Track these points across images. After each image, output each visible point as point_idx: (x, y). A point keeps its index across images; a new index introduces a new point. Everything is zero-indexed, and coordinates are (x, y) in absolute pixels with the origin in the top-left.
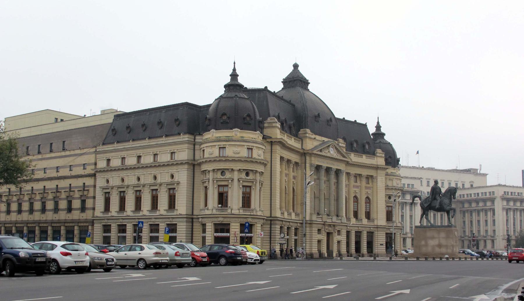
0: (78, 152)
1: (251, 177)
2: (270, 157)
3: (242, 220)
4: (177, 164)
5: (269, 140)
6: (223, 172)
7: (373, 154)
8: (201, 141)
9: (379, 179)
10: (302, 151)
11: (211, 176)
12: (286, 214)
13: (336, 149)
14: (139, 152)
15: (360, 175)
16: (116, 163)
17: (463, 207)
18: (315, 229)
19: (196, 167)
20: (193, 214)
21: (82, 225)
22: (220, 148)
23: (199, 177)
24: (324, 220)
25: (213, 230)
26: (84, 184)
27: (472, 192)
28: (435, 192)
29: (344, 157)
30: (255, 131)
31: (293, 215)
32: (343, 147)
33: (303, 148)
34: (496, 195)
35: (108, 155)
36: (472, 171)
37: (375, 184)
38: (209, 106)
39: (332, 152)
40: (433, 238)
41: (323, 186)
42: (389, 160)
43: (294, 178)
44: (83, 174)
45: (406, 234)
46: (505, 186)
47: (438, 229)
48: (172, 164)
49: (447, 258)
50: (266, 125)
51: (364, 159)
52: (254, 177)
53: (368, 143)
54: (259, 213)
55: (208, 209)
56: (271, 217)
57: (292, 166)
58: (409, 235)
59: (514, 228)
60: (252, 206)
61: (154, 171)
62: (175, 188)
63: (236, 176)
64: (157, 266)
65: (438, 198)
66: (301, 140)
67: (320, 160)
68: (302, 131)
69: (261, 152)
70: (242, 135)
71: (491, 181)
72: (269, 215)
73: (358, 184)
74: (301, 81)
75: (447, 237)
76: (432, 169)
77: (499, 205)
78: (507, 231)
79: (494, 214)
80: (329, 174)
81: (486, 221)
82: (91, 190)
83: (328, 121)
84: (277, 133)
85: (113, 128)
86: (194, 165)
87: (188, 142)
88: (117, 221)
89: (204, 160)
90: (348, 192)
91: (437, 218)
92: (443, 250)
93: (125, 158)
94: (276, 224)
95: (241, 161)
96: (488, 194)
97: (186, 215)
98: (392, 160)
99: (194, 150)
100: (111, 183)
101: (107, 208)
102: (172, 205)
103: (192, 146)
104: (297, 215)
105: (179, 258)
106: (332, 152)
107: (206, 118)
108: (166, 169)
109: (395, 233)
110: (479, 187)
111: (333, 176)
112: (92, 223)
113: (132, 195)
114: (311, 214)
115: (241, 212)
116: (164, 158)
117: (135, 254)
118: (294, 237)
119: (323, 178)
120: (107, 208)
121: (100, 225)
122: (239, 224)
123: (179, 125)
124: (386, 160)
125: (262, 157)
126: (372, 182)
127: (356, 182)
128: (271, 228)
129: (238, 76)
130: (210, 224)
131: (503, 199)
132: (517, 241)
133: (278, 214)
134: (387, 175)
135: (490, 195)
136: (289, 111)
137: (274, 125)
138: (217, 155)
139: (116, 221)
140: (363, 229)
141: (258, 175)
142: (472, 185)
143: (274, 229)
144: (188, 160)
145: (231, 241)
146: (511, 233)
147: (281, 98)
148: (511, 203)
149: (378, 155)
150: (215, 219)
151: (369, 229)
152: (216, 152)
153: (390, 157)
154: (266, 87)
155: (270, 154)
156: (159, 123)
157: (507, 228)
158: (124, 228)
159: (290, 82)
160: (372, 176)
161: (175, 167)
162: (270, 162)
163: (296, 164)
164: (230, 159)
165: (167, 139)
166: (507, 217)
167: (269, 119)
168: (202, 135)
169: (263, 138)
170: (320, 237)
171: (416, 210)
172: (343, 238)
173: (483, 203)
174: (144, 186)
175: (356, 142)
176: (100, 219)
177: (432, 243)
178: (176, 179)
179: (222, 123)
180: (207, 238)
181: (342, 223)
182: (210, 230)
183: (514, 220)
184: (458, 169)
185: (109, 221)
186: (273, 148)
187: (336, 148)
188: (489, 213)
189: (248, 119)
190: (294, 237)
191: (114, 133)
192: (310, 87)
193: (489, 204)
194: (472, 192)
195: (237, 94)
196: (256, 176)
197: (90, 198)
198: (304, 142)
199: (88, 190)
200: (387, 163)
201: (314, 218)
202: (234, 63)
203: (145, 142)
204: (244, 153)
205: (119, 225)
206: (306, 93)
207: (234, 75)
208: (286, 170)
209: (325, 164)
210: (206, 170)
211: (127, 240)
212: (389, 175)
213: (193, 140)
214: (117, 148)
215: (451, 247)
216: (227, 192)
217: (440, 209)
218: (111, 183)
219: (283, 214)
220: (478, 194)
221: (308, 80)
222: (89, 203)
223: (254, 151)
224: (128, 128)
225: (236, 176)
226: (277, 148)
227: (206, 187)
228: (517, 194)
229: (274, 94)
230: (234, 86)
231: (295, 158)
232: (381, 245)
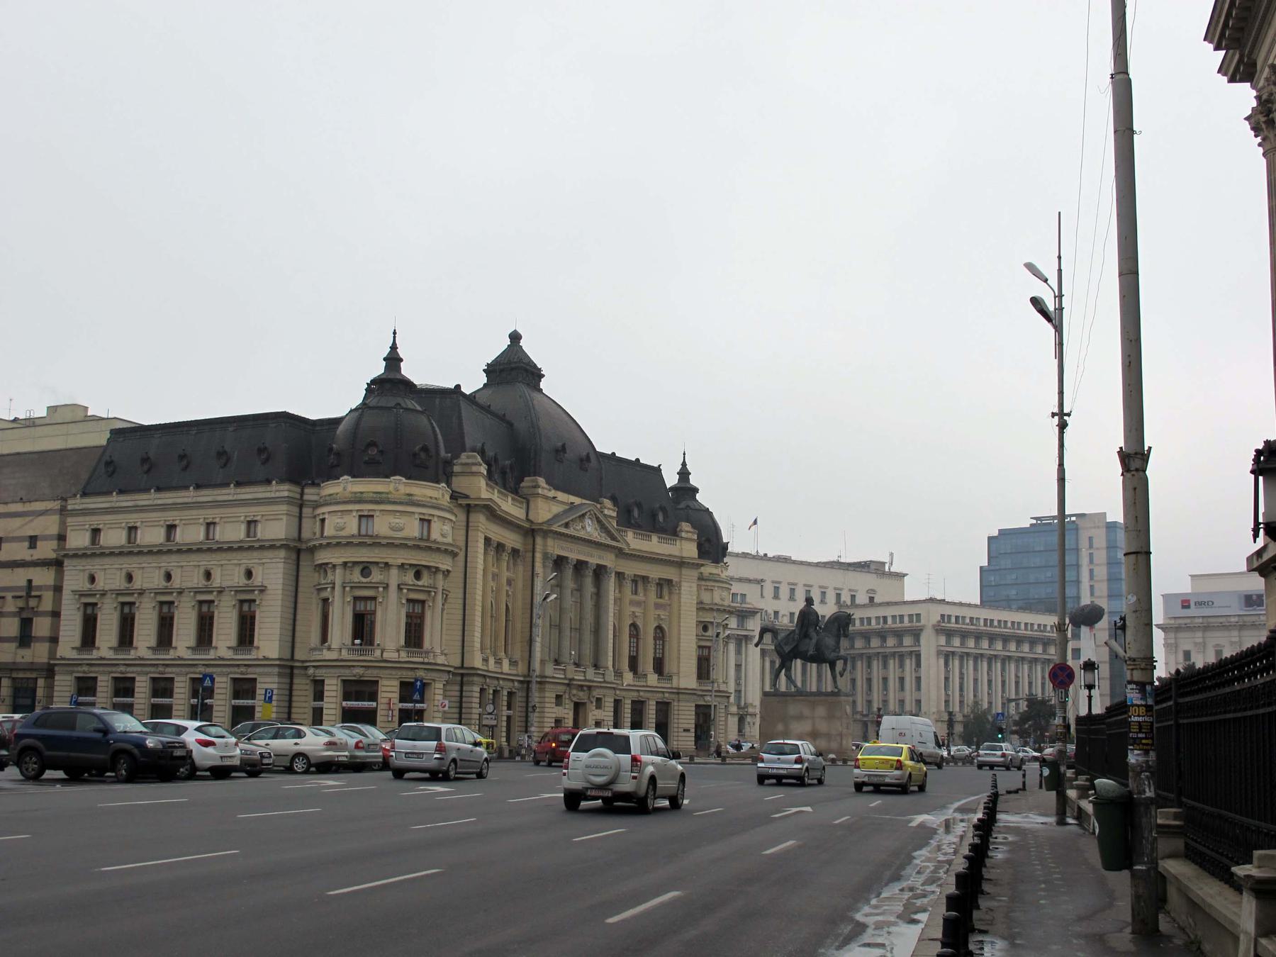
0: (18, 507)
1: (425, 581)
3: (405, 673)
4: (262, 548)
5: (464, 502)
6: (366, 569)
7: (672, 532)
8: (315, 498)
9: (685, 587)
10: (527, 525)
11: (338, 576)
12: (492, 661)
13: (599, 521)
14: (171, 517)
15: (645, 579)
16: (114, 537)
18: (550, 696)
19: (302, 556)
20: (292, 659)
21: (21, 675)
22: (360, 516)
23: (309, 578)
24: (570, 676)
25: (340, 694)
26: (30, 581)
27: (873, 613)
29: (614, 539)
30: (438, 482)
31: (506, 664)
33: (531, 517)
34: (923, 622)
35: (95, 521)
36: (873, 567)
37: (675, 597)
38: (336, 422)
39: (590, 529)
40: (800, 717)
41: (569, 601)
42: (707, 545)
43: (509, 582)
44: (28, 558)
46: (943, 601)
47: (812, 698)
48: (251, 548)
49: (833, 761)
50: (456, 469)
51: (654, 545)
52: (431, 582)
53: (663, 509)
54: (441, 660)
55: (329, 649)
57: (505, 557)
59: (961, 695)
60: (427, 645)
61: (205, 561)
62: (254, 601)
63: (394, 577)
64: (326, 767)
65: (813, 634)
66: (525, 499)
67: (565, 545)
68: (527, 482)
69: (447, 528)
70: (408, 490)
71: (913, 590)
72: (458, 664)
73: (641, 597)
74: (526, 371)
75: (830, 717)
76: (785, 560)
77: (929, 645)
78: (947, 702)
79: (918, 665)
80: (582, 576)
81: (902, 680)
82: (48, 596)
84: (481, 488)
85: (106, 458)
86: (299, 552)
87: (289, 501)
88: (114, 669)
89: (324, 542)
90: (619, 615)
91: (805, 675)
93: (136, 528)
94: (472, 683)
95: (405, 546)
96: (906, 619)
97: (279, 659)
98: (712, 545)
99: (300, 518)
100: (100, 584)
101: (88, 639)
102: (246, 635)
103: (296, 510)
104: (513, 663)
105: (362, 753)
106: (590, 529)
107: (331, 449)
108: (236, 557)
110: (888, 604)
111: (589, 582)
112: (49, 671)
113: (151, 611)
114: (543, 662)
116: (232, 532)
117: (286, 745)
118: (505, 712)
119: (570, 583)
120: (88, 639)
121: (68, 678)
122: (397, 683)
123: (267, 460)
124: (700, 547)
125: (449, 540)
126: (670, 593)
127: (636, 593)
128: (461, 691)
130: (334, 681)
131: (939, 630)
132: (966, 726)
133: (478, 663)
134: (701, 578)
135: (911, 621)
136: (491, 435)
137: (474, 469)
138: (355, 532)
139: (109, 669)
140: (648, 695)
141: (440, 576)
142: (871, 599)
144: (286, 539)
145: (379, 718)
146: (956, 708)
147: (486, 409)
148: (956, 642)
149: (683, 535)
150: (347, 671)
152: (351, 526)
153: (708, 540)
155: (464, 532)
156: (221, 454)
157: (947, 695)
158: (128, 684)
159: (502, 371)
160: (669, 582)
161: (255, 554)
163: (515, 552)
164: (384, 542)
165: (238, 490)
166: (947, 672)
167: (464, 455)
168: (318, 485)
169: (451, 497)
173: (899, 638)
174: (180, 593)
175: (639, 505)
176: (70, 665)
178: (258, 579)
179: (366, 463)
180: (325, 711)
182: (334, 694)
183: (962, 678)
184: (842, 560)
185: (93, 669)
187: (597, 518)
188: (908, 662)
189: (423, 455)
190: (505, 712)
191: (111, 469)
192: (543, 384)
193: (908, 641)
194: (873, 613)
195: (399, 400)
197: (44, 614)
198: (532, 505)
199: (39, 597)
200: (703, 553)
201: (550, 670)
202: (395, 333)
203: (187, 494)
204: (412, 529)
205: (115, 679)
206: (535, 395)
207: (393, 360)
208: (508, 569)
209: (574, 553)
211: (215, 714)
213: (298, 496)
214: (117, 504)
216: (374, 613)
217: (818, 658)
218: (100, 584)
219: (486, 660)
222: (41, 627)
223: (433, 524)
224: (145, 460)
225: (394, 577)
226: (480, 520)
227: (325, 601)
228: (968, 621)
229: (471, 399)
230: (390, 384)
231: (511, 539)
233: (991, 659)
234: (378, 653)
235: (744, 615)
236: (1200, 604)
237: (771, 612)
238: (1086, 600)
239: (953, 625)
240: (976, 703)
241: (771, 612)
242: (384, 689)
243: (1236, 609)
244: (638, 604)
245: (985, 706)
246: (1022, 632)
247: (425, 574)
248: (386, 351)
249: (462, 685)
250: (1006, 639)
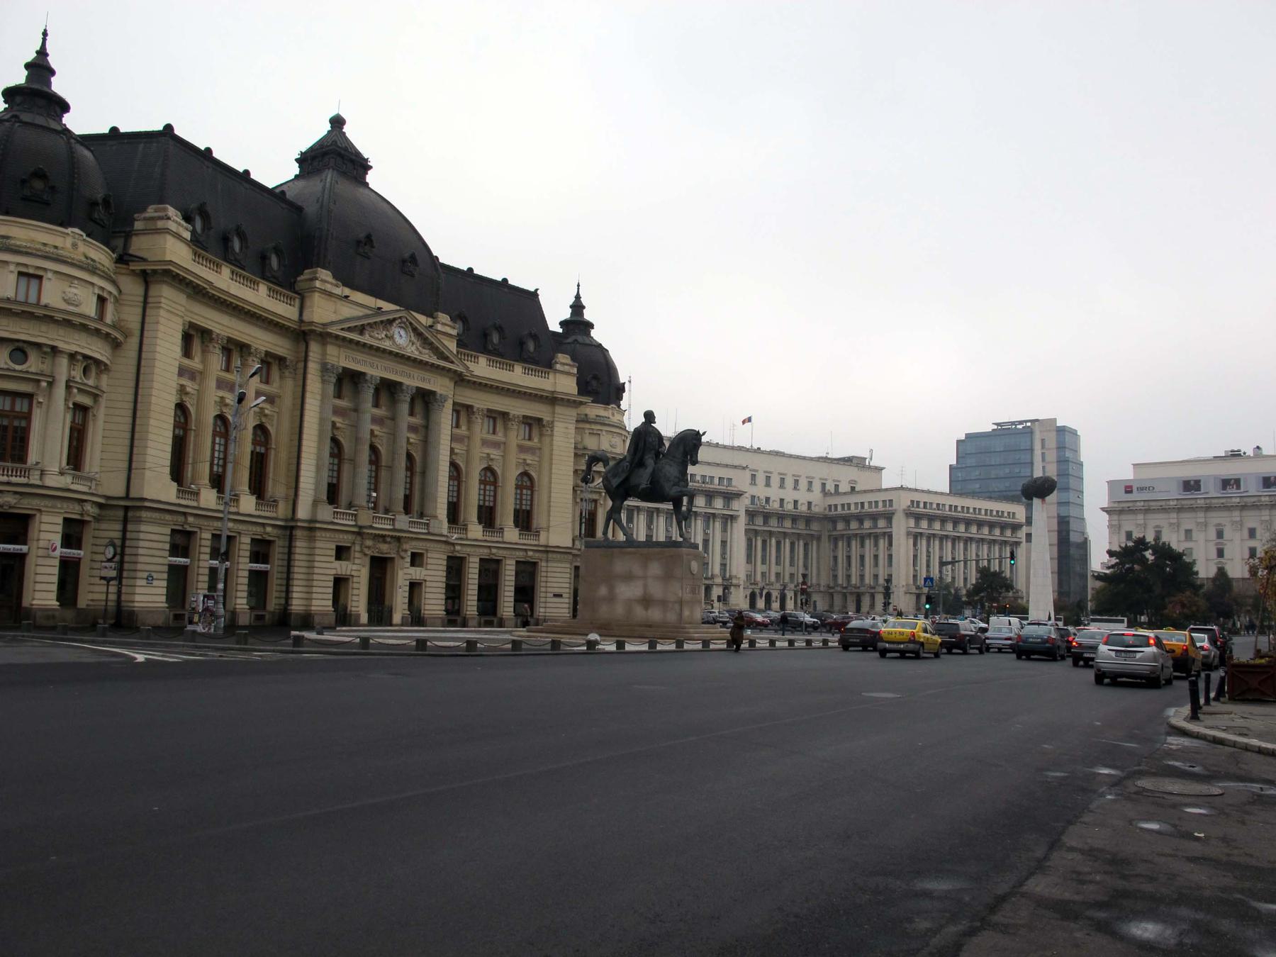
1: (34, 364)
2: (139, 318)
9: (559, 428)
17: (835, 529)
27: (853, 499)
28: (641, 445)
32: (450, 335)
34: (895, 506)
37: (547, 440)
39: (401, 340)
40: (629, 578)
45: (713, 577)
47: (645, 551)
50: (138, 225)
51: (518, 376)
56: (127, 497)
58: (719, 580)
65: (650, 462)
71: (888, 481)
72: (120, 492)
73: (500, 437)
74: (340, 155)
75: (668, 577)
77: (901, 526)
79: (890, 544)
81: (876, 557)
83: (404, 261)
92: (655, 614)
96: (880, 504)
98: (601, 381)
106: (401, 340)
109: (229, 537)
114: (315, 503)
115: (66, 481)
122: (60, 521)
126: (541, 435)
128: (124, 531)
129: (53, 73)
131: (908, 514)
135: (885, 506)
142: (853, 489)
143: (134, 535)
148: (924, 524)
151: (259, 529)
154: (169, 128)
155: (140, 310)
159: (314, 158)
160: (539, 420)
162: (137, 333)
166: (916, 550)
170: (343, 568)
171: (735, 531)
172: (434, 575)
175: (499, 329)
177: (629, 591)
181: (429, 533)
183: (928, 556)
186: (151, 293)
188: (881, 542)
192: (371, 178)
194: (853, 499)
196: (53, 365)
198: (308, 303)
202: (45, 34)
209: (376, 370)
212: (590, 423)
215: (677, 607)
217: (653, 493)
220: (862, 504)
225: (62, 369)
226: (168, 296)
231: (279, 345)
232: (556, 596)
233: (955, 540)
235: (730, 497)
236: (1141, 489)
237: (763, 497)
238: (1038, 473)
239: (921, 510)
240: (941, 578)
241: (763, 497)
243: (1175, 493)
244: (496, 445)
245: (949, 580)
246: (982, 517)
248: (31, 56)
249: (125, 521)
250: (968, 523)
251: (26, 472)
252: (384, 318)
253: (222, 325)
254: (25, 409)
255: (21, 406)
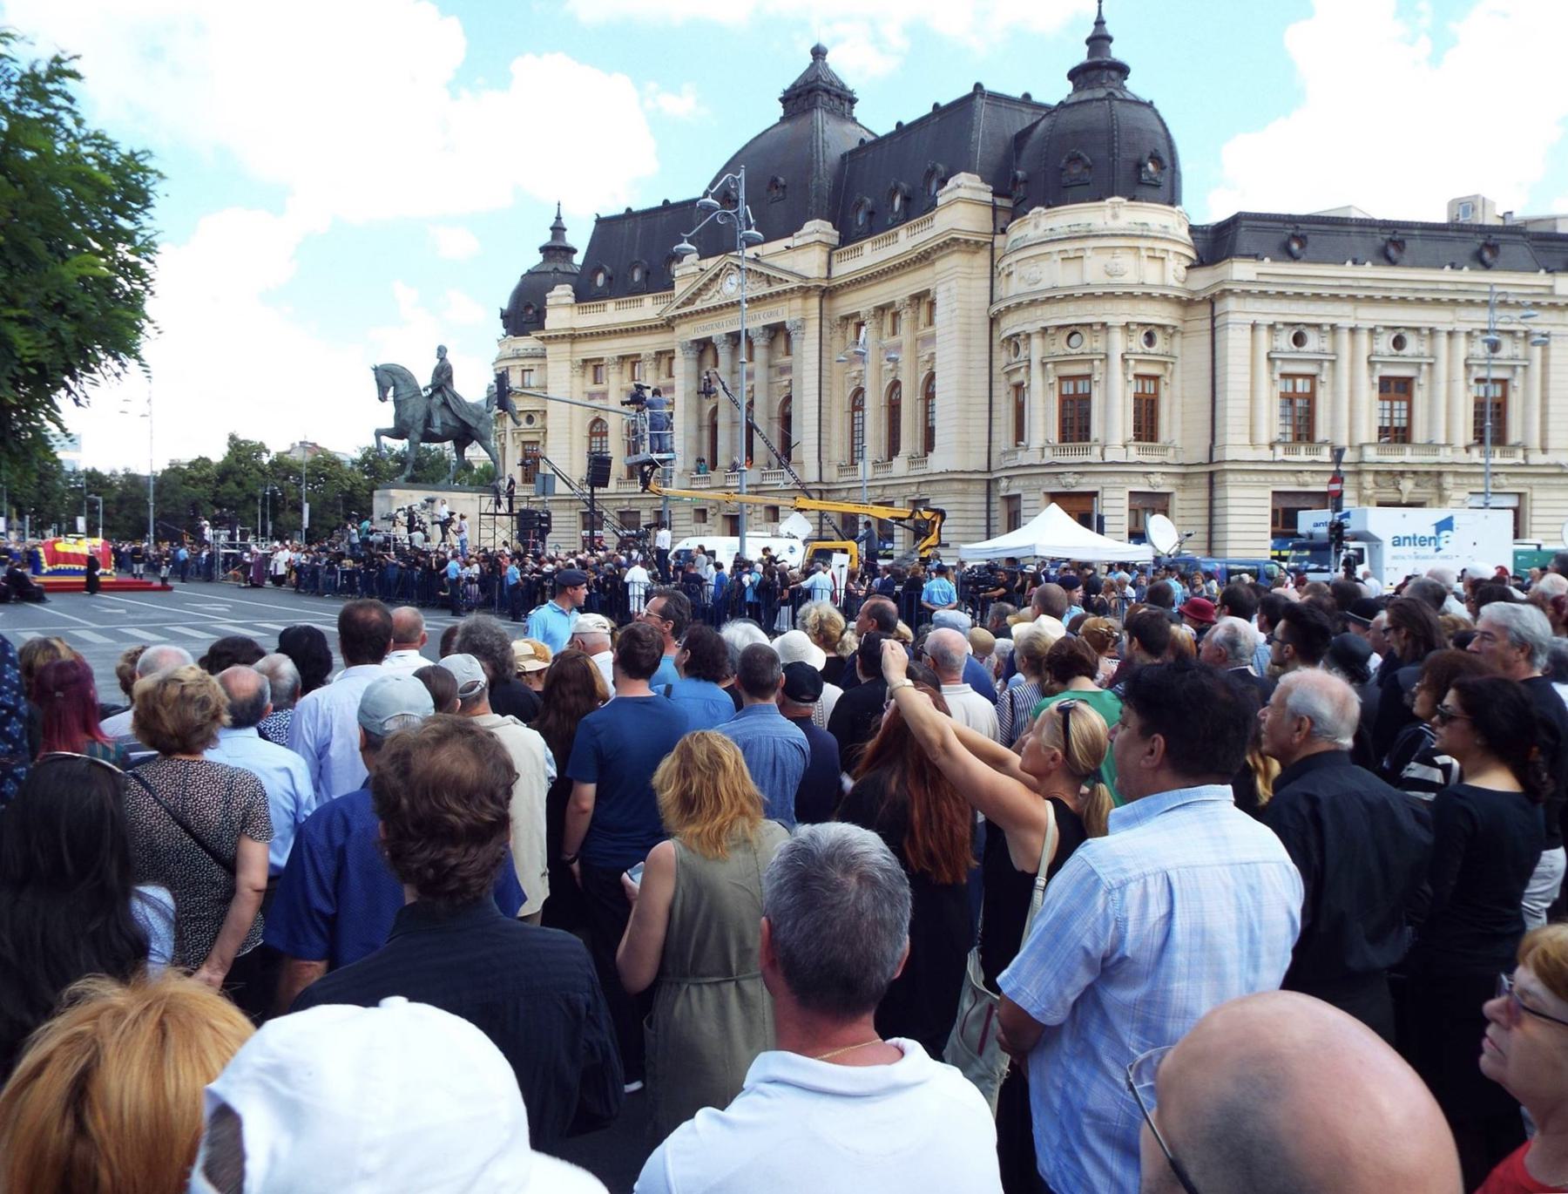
1: (1160, 344)
6: (1072, 331)
39: (731, 288)
52: (1166, 348)
115: (1133, 454)
129: (1110, 39)
141: (1443, 340)
159: (799, 96)
164: (1099, 291)
192: (858, 111)
196: (1107, 342)
207: (1099, 41)
209: (716, 329)
210: (1018, 335)
221: (851, 92)
225: (1118, 343)
227: (1018, 387)
234: (1097, 450)
242: (1198, 512)
247: (1159, 336)
251: (1088, 450)
252: (711, 275)
253: (609, 349)
254: (1307, 390)
255: (1150, 388)
